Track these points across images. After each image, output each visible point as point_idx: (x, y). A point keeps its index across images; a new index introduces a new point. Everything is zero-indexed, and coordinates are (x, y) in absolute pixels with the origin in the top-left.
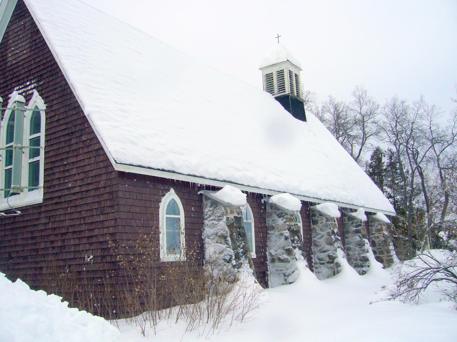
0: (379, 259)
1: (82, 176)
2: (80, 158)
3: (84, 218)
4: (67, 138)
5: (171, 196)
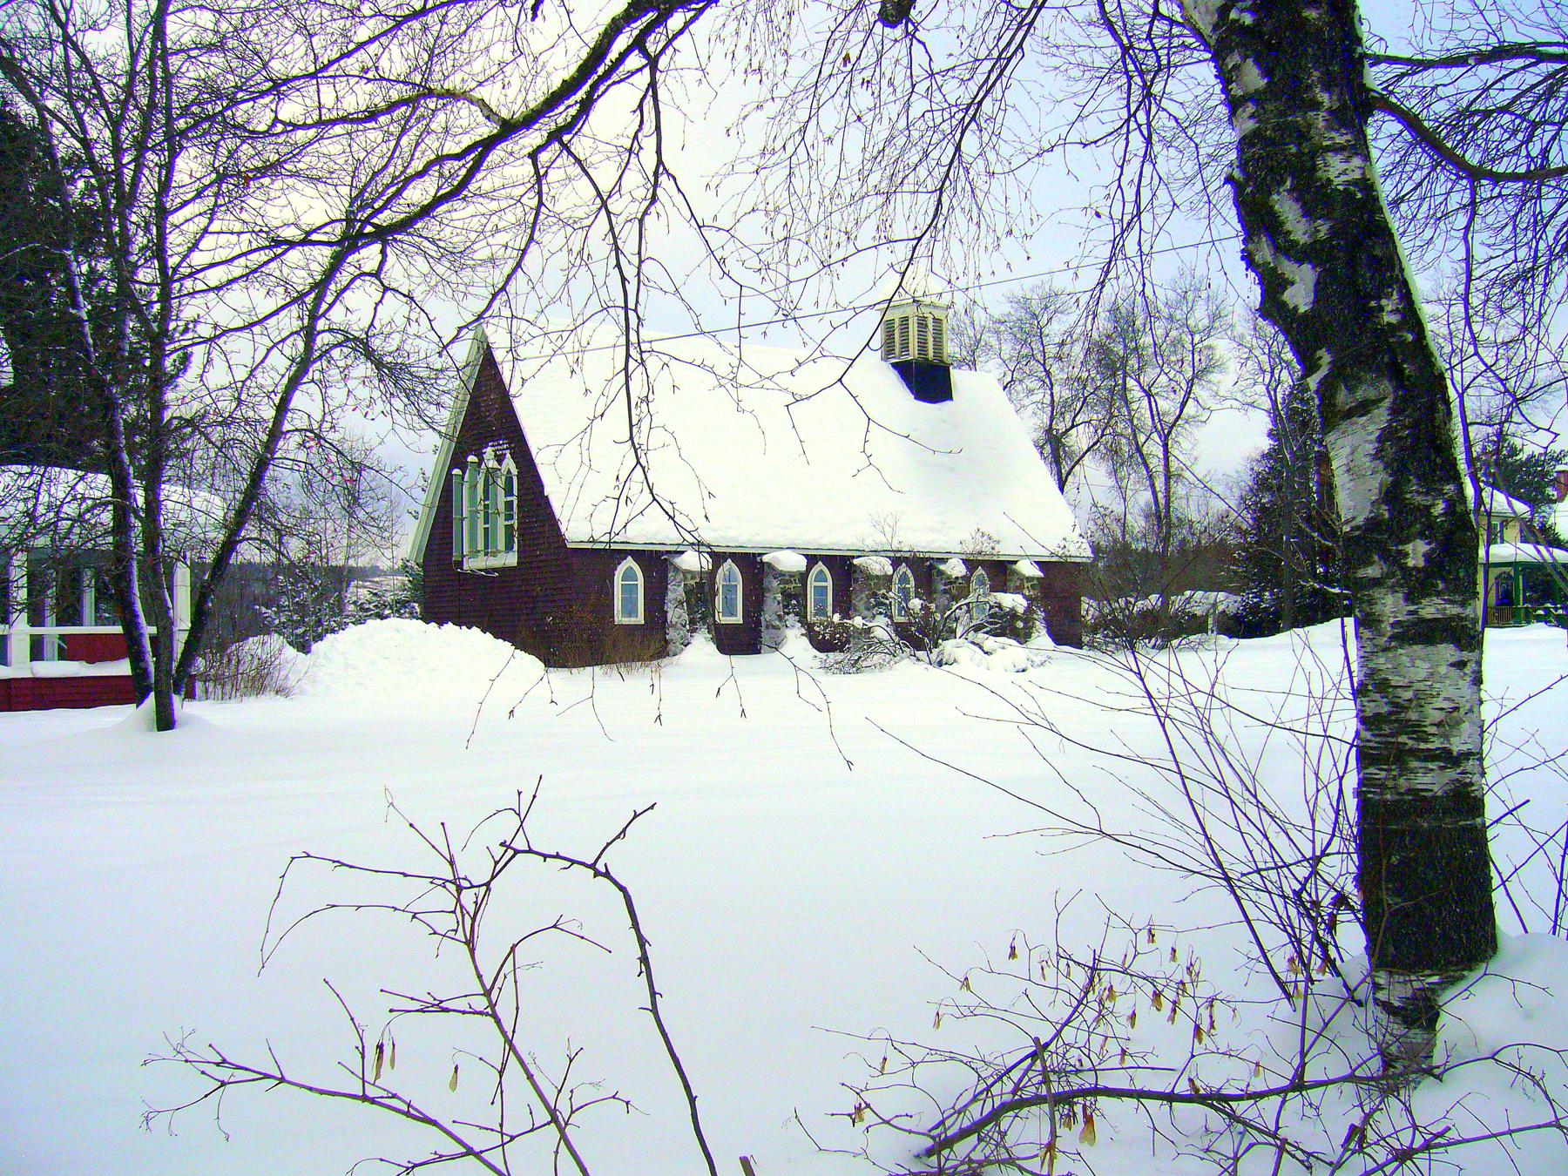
5: (629, 562)
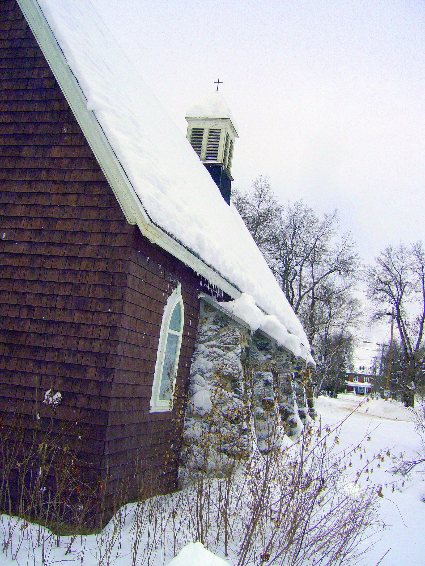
1: (38, 224)
2: (39, 188)
3: (31, 309)
4: (12, 142)
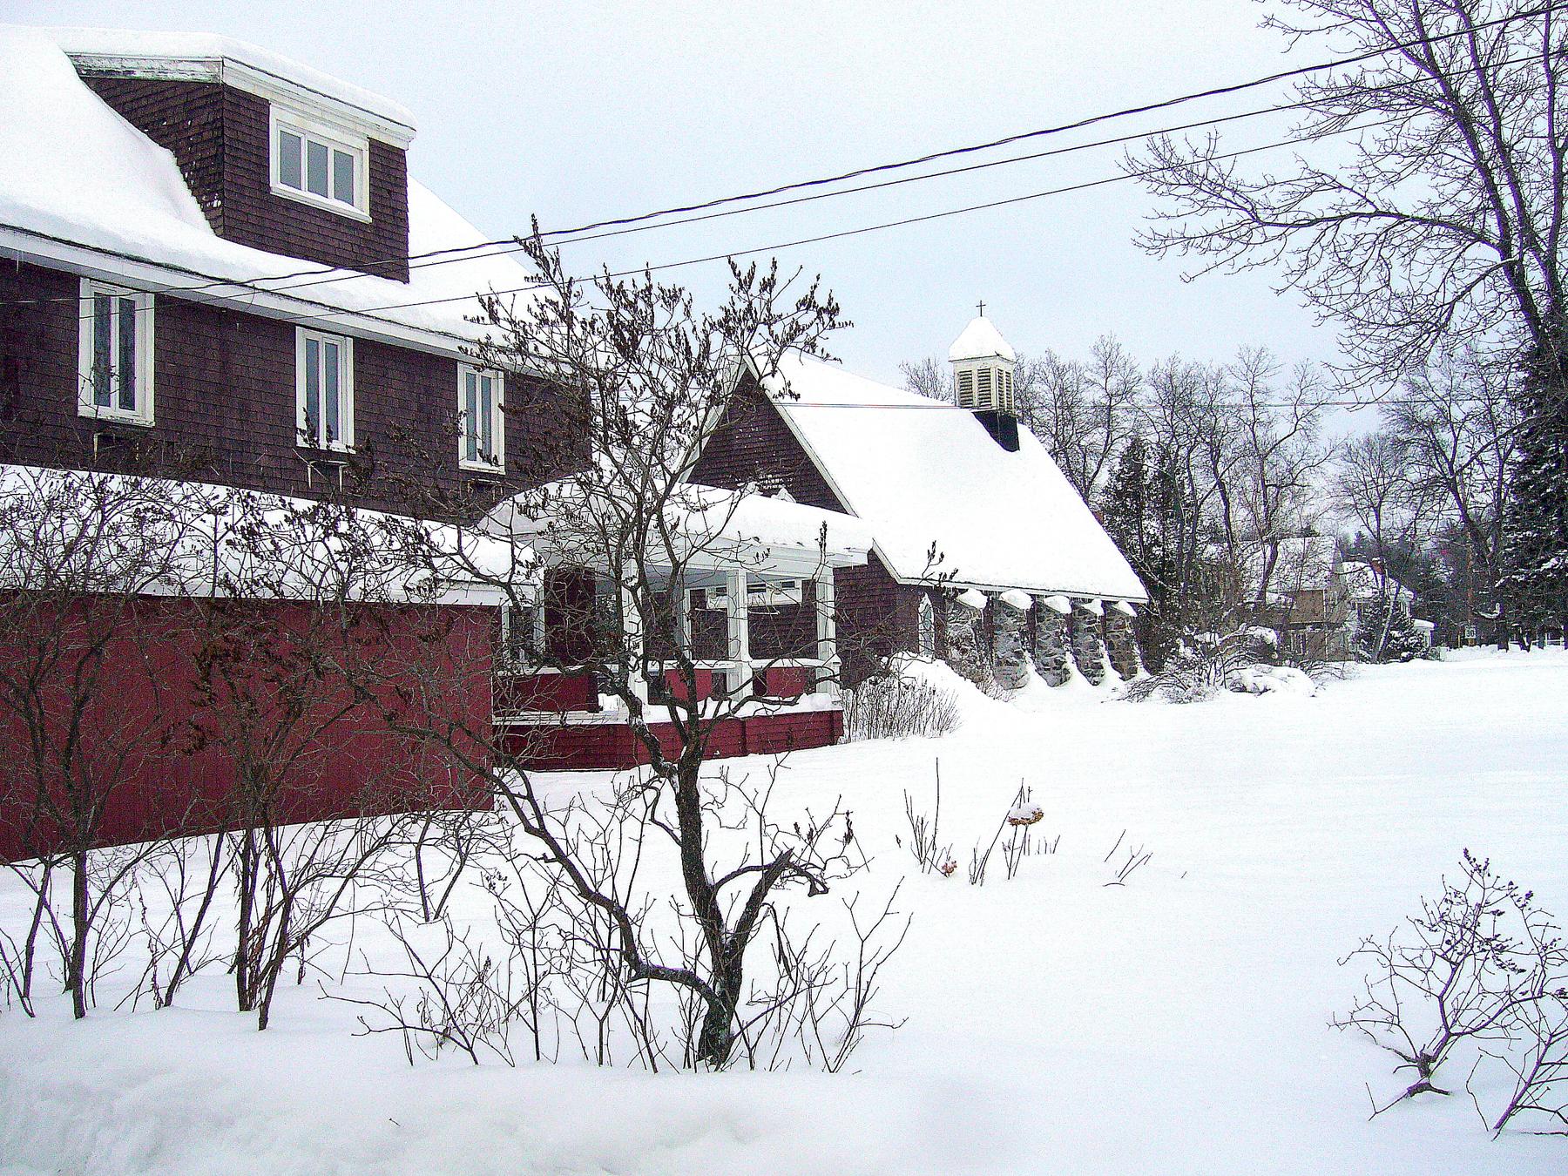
0: (1115, 667)
